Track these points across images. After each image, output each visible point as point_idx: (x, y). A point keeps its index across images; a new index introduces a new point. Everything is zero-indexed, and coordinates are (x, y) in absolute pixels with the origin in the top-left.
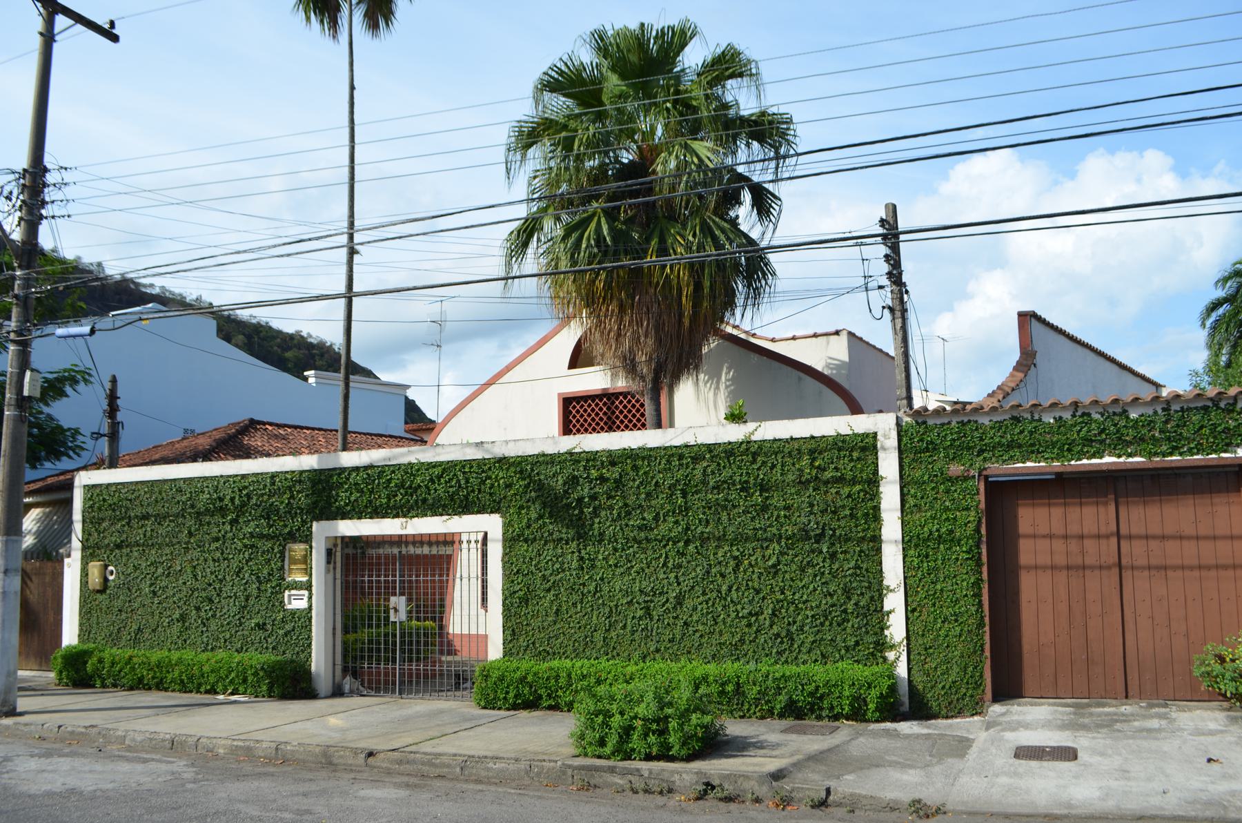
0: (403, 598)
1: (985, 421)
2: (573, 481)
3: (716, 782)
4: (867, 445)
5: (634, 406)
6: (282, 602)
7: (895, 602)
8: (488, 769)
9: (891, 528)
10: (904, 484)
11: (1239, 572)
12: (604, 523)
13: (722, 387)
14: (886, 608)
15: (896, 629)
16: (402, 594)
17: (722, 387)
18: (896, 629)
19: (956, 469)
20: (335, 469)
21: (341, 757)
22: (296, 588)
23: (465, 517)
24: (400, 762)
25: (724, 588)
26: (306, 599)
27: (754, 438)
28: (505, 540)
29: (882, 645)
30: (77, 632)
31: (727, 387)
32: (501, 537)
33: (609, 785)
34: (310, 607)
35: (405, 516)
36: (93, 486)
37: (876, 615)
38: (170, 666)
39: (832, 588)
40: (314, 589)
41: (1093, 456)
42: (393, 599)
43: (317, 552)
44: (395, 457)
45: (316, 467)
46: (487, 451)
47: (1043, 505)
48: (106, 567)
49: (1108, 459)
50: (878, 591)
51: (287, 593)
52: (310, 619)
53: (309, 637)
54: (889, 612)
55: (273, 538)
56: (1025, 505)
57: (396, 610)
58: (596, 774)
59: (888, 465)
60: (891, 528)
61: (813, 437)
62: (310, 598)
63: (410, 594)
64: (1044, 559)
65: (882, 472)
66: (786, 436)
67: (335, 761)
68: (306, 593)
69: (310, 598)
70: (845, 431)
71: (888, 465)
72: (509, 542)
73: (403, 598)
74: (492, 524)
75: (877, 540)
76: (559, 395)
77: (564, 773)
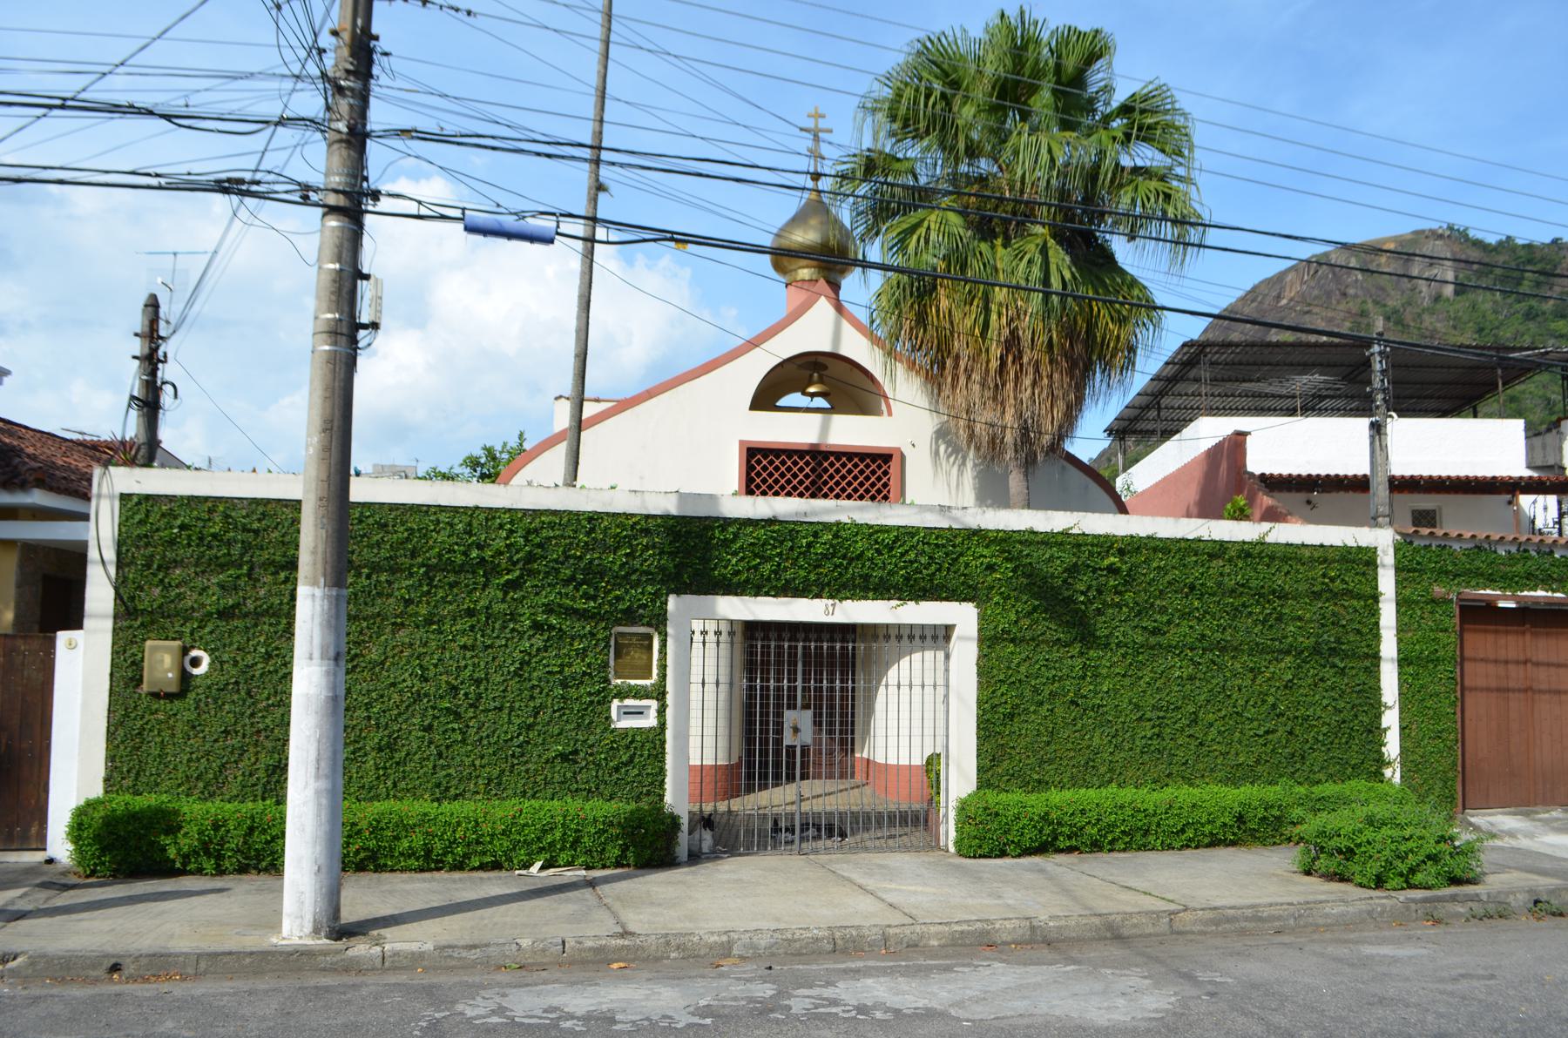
0: (809, 714)
1: (1456, 546)
2: (1073, 570)
3: (1544, 898)
4: (1365, 560)
5: (771, 475)
6: (608, 718)
7: (1391, 720)
8: (1327, 916)
9: (1389, 647)
10: (1402, 603)
11: (1564, 697)
12: (1116, 625)
13: (969, 464)
14: (1384, 725)
15: (1392, 746)
16: (806, 707)
17: (969, 464)
18: (1392, 746)
19: (1438, 590)
20: (717, 519)
21: (1135, 926)
22: (635, 697)
23: (923, 604)
24: (1216, 922)
25: (1240, 702)
26: (653, 713)
27: (1269, 539)
28: (981, 640)
29: (1381, 762)
30: (101, 772)
31: (975, 465)
32: (975, 634)
33: (1458, 915)
34: (662, 726)
35: (831, 597)
36: (148, 497)
37: (1375, 732)
38: (403, 827)
39: (1341, 704)
40: (669, 699)
41: (1531, 589)
42: (789, 716)
43: (677, 640)
44: (815, 513)
45: (674, 511)
46: (955, 519)
47: (1517, 632)
48: (185, 651)
49: (1540, 593)
50: (1376, 708)
51: (616, 703)
52: (663, 742)
53: (662, 771)
54: (1385, 730)
55: (593, 617)
56: (1475, 631)
57: (796, 730)
58: (1439, 905)
59: (1387, 582)
60: (1389, 647)
61: (1322, 546)
62: (661, 712)
63: (818, 707)
64: (1481, 682)
65: (1381, 588)
66: (1297, 541)
67: (1125, 932)
68: (654, 704)
69: (661, 712)
70: (1351, 543)
71: (1387, 582)
72: (989, 640)
73: (809, 714)
74: (963, 617)
75: (1376, 657)
76: (741, 442)
77: (1408, 909)
